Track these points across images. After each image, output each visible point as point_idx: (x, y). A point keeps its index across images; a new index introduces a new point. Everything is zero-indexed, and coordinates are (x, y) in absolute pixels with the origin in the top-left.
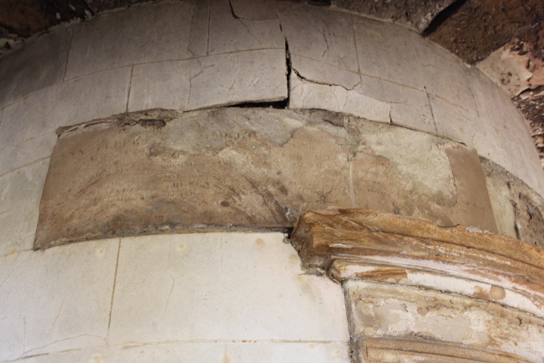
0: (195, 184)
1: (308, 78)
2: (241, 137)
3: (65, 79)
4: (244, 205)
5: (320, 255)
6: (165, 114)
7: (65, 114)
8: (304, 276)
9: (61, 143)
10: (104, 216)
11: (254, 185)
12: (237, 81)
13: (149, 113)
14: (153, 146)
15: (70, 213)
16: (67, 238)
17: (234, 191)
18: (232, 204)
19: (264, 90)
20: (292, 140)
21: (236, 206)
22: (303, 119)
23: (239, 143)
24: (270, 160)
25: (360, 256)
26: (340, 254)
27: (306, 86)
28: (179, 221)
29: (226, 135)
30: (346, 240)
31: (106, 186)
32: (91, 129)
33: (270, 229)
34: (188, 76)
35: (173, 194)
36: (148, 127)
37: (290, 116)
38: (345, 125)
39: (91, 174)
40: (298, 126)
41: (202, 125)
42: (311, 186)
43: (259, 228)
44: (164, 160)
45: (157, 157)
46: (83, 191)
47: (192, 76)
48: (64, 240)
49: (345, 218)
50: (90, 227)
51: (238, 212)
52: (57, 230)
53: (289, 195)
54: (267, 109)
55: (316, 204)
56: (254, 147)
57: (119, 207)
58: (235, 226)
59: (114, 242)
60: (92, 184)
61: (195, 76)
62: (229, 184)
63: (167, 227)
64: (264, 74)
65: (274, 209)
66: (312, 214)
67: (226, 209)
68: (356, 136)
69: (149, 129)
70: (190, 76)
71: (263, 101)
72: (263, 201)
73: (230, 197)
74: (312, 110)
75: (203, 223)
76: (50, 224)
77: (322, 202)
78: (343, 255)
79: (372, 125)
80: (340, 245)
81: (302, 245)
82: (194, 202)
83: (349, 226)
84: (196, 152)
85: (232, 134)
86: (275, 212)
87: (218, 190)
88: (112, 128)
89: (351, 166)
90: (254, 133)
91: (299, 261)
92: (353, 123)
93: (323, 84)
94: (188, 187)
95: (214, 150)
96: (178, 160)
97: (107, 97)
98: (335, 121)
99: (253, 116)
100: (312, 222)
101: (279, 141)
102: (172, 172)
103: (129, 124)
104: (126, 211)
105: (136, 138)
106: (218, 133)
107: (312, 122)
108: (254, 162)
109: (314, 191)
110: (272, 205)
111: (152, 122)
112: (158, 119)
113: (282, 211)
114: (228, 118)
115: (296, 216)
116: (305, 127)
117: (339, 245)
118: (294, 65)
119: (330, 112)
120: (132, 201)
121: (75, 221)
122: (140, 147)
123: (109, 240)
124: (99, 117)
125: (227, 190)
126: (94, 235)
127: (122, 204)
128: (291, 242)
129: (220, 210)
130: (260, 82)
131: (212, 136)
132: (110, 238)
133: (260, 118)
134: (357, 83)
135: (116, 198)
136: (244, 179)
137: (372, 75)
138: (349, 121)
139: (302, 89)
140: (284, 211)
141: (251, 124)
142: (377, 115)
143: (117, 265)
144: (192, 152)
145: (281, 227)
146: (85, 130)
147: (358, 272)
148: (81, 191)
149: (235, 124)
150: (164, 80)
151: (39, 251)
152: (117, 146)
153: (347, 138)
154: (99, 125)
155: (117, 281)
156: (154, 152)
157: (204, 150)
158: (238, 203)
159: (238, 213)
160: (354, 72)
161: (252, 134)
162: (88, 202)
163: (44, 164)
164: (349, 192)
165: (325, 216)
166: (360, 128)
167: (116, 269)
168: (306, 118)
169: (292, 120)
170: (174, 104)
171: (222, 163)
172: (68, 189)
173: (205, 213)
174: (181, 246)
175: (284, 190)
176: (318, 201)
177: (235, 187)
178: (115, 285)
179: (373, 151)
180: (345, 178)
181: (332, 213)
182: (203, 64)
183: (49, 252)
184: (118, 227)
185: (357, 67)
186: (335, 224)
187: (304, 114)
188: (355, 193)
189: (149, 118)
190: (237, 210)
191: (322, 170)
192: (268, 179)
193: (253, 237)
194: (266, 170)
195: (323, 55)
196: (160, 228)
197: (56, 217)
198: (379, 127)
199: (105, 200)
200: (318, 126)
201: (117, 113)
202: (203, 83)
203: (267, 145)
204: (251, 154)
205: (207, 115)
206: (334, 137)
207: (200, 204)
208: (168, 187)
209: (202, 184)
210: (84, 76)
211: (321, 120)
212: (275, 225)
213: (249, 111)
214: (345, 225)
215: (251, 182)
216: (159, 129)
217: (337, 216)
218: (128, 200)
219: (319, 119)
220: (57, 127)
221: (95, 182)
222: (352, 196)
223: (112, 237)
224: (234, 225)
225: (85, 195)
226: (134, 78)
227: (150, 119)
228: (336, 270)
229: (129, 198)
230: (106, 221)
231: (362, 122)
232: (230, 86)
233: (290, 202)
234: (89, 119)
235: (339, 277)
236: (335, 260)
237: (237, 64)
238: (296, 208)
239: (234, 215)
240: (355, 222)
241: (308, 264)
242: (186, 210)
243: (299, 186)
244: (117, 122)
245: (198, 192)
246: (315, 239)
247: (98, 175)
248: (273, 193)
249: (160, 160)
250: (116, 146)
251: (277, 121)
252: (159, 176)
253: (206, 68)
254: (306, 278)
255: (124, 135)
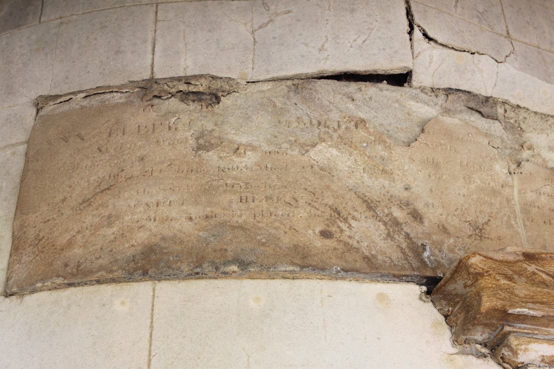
0: (275, 199)
1: (440, 41)
2: (344, 127)
3: (42, 20)
4: (356, 238)
5: (486, 325)
6: (217, 85)
7: (45, 76)
8: (456, 356)
9: (43, 122)
10: (127, 245)
11: (370, 206)
12: (329, 39)
13: (193, 82)
14: (201, 135)
15: (68, 236)
16: (65, 278)
17: (339, 214)
18: (337, 235)
19: (374, 54)
20: (422, 136)
21: (344, 238)
22: (436, 104)
23: (340, 137)
24: (391, 167)
25: (548, 329)
26: (519, 325)
27: (437, 51)
28: (253, 258)
29: (320, 124)
30: (533, 303)
31: (126, 195)
32: (95, 101)
33: (399, 278)
34: (249, 25)
35: (241, 215)
36: (191, 103)
37: (415, 98)
38: (501, 117)
39: (100, 174)
40: (430, 116)
41: (279, 105)
42: (459, 212)
43: (382, 276)
44: (221, 158)
45: (210, 153)
46: (87, 202)
47: (256, 27)
48: (59, 281)
49: (532, 268)
50: (104, 261)
51: (349, 248)
52: (49, 265)
53: (426, 224)
54: (379, 85)
55: (469, 241)
56: (365, 145)
57: (151, 230)
58: (346, 271)
59: (143, 289)
60: (102, 192)
61: (260, 27)
62: (330, 203)
63: (234, 268)
64: (372, 30)
65: (404, 245)
66: (482, 258)
67: (328, 243)
68: (518, 136)
69: (193, 106)
70: (252, 26)
71: (374, 73)
72: (386, 232)
73: (334, 223)
74: (449, 91)
75: (293, 264)
76: (34, 253)
77: (478, 238)
78: (523, 326)
79: (537, 118)
80: (525, 311)
81: (454, 307)
82: (276, 228)
83: (537, 280)
84: (272, 148)
85: (328, 123)
86: (407, 250)
87: (313, 211)
88: (132, 102)
89: (516, 181)
90: (363, 121)
91: (446, 333)
92: (510, 114)
93: (461, 51)
94: (265, 204)
95: (302, 146)
96: (245, 159)
97: (118, 52)
98: (483, 110)
99: (358, 96)
100: (481, 271)
101: (402, 136)
102: (235, 178)
103: (160, 97)
104: (163, 239)
105: (173, 120)
106: (306, 119)
107: (449, 110)
108: (367, 168)
109: (463, 219)
110: (400, 238)
111: (197, 96)
112: (207, 91)
113: (418, 250)
114: (320, 96)
115: (439, 259)
116: (440, 116)
117: (524, 310)
118: (417, 19)
119: (475, 95)
120: (173, 223)
121: (76, 250)
122: (180, 135)
123: (135, 284)
124: (107, 84)
125: (328, 212)
126: (111, 276)
127: (156, 226)
128: (432, 301)
129: (319, 243)
130: (367, 42)
131: (296, 124)
132: (137, 281)
133: (371, 98)
134: (509, 52)
135: (145, 216)
136: (354, 195)
137: (527, 41)
138: (506, 111)
139: (431, 57)
140: (420, 250)
141: (358, 107)
142: (543, 104)
143: (152, 327)
144: (267, 148)
145: (418, 276)
146: (85, 103)
147: (545, 354)
148: (84, 202)
149: (331, 106)
150: (210, 31)
151: (14, 297)
152: (142, 132)
153: (505, 137)
154: (108, 96)
155: (153, 354)
156: (203, 144)
157: (285, 145)
158: (348, 233)
159: (349, 250)
160: (501, 35)
161: (360, 123)
162: (97, 220)
163: (14, 154)
164: (517, 223)
165: (502, 262)
166: (521, 123)
167: (151, 334)
168: (440, 103)
169: (419, 105)
170: (229, 68)
171: (316, 167)
172: (61, 197)
173: (296, 247)
174: (257, 300)
175: (417, 216)
176: (471, 236)
177: (340, 208)
178: (150, 360)
179: (544, 160)
180: (508, 201)
181: (511, 258)
182: (273, 8)
183: (31, 299)
184: (150, 264)
185: (504, 27)
186: (516, 277)
187: (437, 96)
188: (525, 226)
189: (192, 88)
190: (346, 244)
191: (473, 186)
192: (391, 196)
193: (371, 289)
194: (386, 183)
195: (456, 6)
196: (222, 269)
197: (41, 242)
198: (549, 123)
199: (126, 218)
200: (460, 116)
201: (137, 78)
202: (274, 38)
203: (385, 142)
204: (361, 155)
205: (286, 89)
206: (486, 135)
207: (286, 233)
208: (231, 202)
209: (287, 199)
210: (75, 17)
211: (463, 108)
212: (408, 273)
213: (353, 87)
214: (532, 279)
215: (365, 201)
216: (210, 108)
217: (520, 263)
218: (166, 220)
219: (460, 106)
220: (35, 96)
221: (108, 189)
222: (521, 230)
223: (141, 280)
224: (343, 270)
225: (91, 208)
226: (159, 24)
227: (194, 90)
228: (512, 350)
229: (167, 217)
230: (130, 252)
231: (523, 114)
232: (319, 46)
233: (429, 235)
234: (90, 85)
235: (514, 362)
236: (510, 333)
237: (328, 12)
238: (438, 246)
239: (343, 253)
240: (548, 274)
241: (464, 338)
242: (264, 241)
243: (440, 211)
244: (138, 92)
245: (281, 213)
246: (484, 299)
247: (112, 178)
248: (401, 220)
249: (215, 157)
250: (139, 131)
251: (397, 105)
252: (215, 183)
253: (277, 15)
254: (461, 360)
255: (152, 115)
